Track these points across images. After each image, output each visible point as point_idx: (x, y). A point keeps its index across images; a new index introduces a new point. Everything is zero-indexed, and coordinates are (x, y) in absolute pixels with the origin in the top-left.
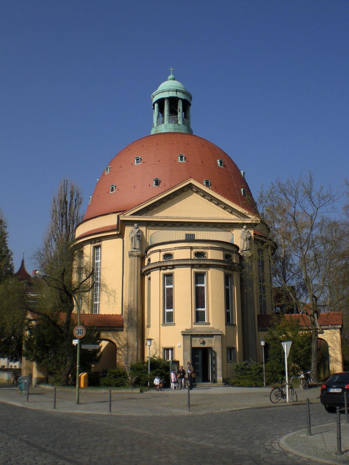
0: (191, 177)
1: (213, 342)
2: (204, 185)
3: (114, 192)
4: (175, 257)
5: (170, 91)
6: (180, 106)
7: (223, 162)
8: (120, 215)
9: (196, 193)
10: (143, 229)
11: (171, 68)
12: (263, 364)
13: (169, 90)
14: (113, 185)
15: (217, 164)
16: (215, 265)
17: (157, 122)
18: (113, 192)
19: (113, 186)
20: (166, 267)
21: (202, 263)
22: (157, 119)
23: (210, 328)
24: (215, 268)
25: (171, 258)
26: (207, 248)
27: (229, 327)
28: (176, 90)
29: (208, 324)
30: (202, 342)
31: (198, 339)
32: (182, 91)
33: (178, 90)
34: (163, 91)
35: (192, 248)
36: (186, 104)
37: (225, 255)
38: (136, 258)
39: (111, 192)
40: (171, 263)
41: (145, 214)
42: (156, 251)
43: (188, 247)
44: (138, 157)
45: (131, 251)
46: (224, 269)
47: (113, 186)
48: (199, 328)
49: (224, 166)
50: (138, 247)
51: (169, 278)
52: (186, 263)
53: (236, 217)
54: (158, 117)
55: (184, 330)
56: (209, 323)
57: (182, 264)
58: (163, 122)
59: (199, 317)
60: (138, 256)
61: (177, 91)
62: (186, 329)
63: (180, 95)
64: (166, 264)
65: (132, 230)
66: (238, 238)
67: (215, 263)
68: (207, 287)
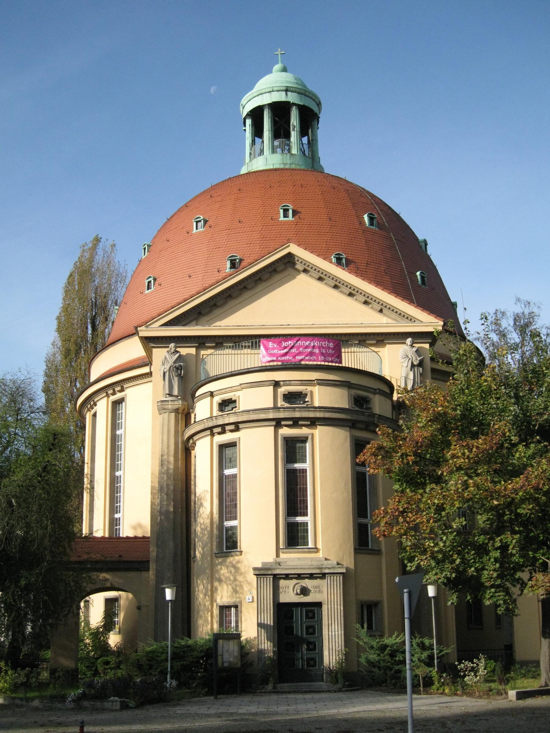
0: (289, 241)
1: (325, 590)
2: (331, 262)
3: (152, 289)
4: (242, 406)
5: (273, 91)
6: (294, 119)
7: (376, 218)
8: (140, 327)
9: (304, 273)
10: (188, 351)
11: (279, 50)
12: (433, 638)
13: (271, 90)
14: (150, 277)
15: (362, 222)
16: (330, 419)
17: (250, 154)
18: (149, 291)
19: (150, 280)
20: (223, 429)
21: (297, 415)
22: (251, 150)
23: (319, 560)
24: (342, 428)
25: (233, 408)
26: (309, 383)
27: (364, 558)
28: (284, 88)
29: (316, 550)
30: (299, 591)
31: (291, 583)
32: (298, 90)
33: (289, 89)
34: (261, 92)
35: (276, 384)
36: (309, 119)
37: (354, 398)
38: (173, 415)
39: (147, 292)
40: (233, 419)
41: (195, 322)
42: (203, 396)
43: (268, 383)
44: (199, 218)
45: (162, 401)
46: (350, 427)
47: (150, 280)
48: (293, 560)
49: (379, 226)
50: (176, 392)
51: (226, 453)
52: (263, 416)
53: (390, 321)
54: (253, 142)
55: (260, 566)
56: (316, 548)
57: (256, 421)
58: (262, 152)
59: (294, 536)
60: (176, 411)
61: (287, 90)
62: (262, 563)
63: (292, 98)
64: (220, 422)
65: (166, 358)
66: (394, 364)
67: (328, 415)
68: (311, 468)
